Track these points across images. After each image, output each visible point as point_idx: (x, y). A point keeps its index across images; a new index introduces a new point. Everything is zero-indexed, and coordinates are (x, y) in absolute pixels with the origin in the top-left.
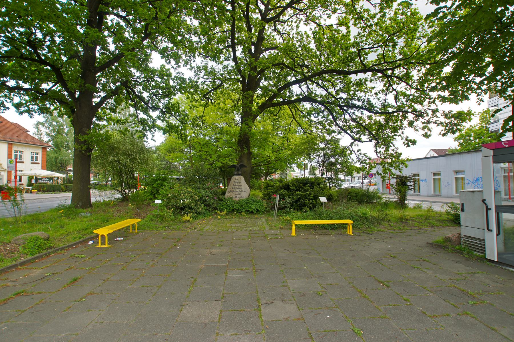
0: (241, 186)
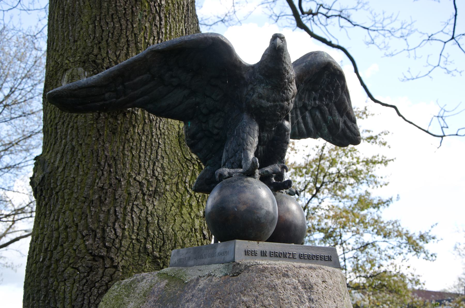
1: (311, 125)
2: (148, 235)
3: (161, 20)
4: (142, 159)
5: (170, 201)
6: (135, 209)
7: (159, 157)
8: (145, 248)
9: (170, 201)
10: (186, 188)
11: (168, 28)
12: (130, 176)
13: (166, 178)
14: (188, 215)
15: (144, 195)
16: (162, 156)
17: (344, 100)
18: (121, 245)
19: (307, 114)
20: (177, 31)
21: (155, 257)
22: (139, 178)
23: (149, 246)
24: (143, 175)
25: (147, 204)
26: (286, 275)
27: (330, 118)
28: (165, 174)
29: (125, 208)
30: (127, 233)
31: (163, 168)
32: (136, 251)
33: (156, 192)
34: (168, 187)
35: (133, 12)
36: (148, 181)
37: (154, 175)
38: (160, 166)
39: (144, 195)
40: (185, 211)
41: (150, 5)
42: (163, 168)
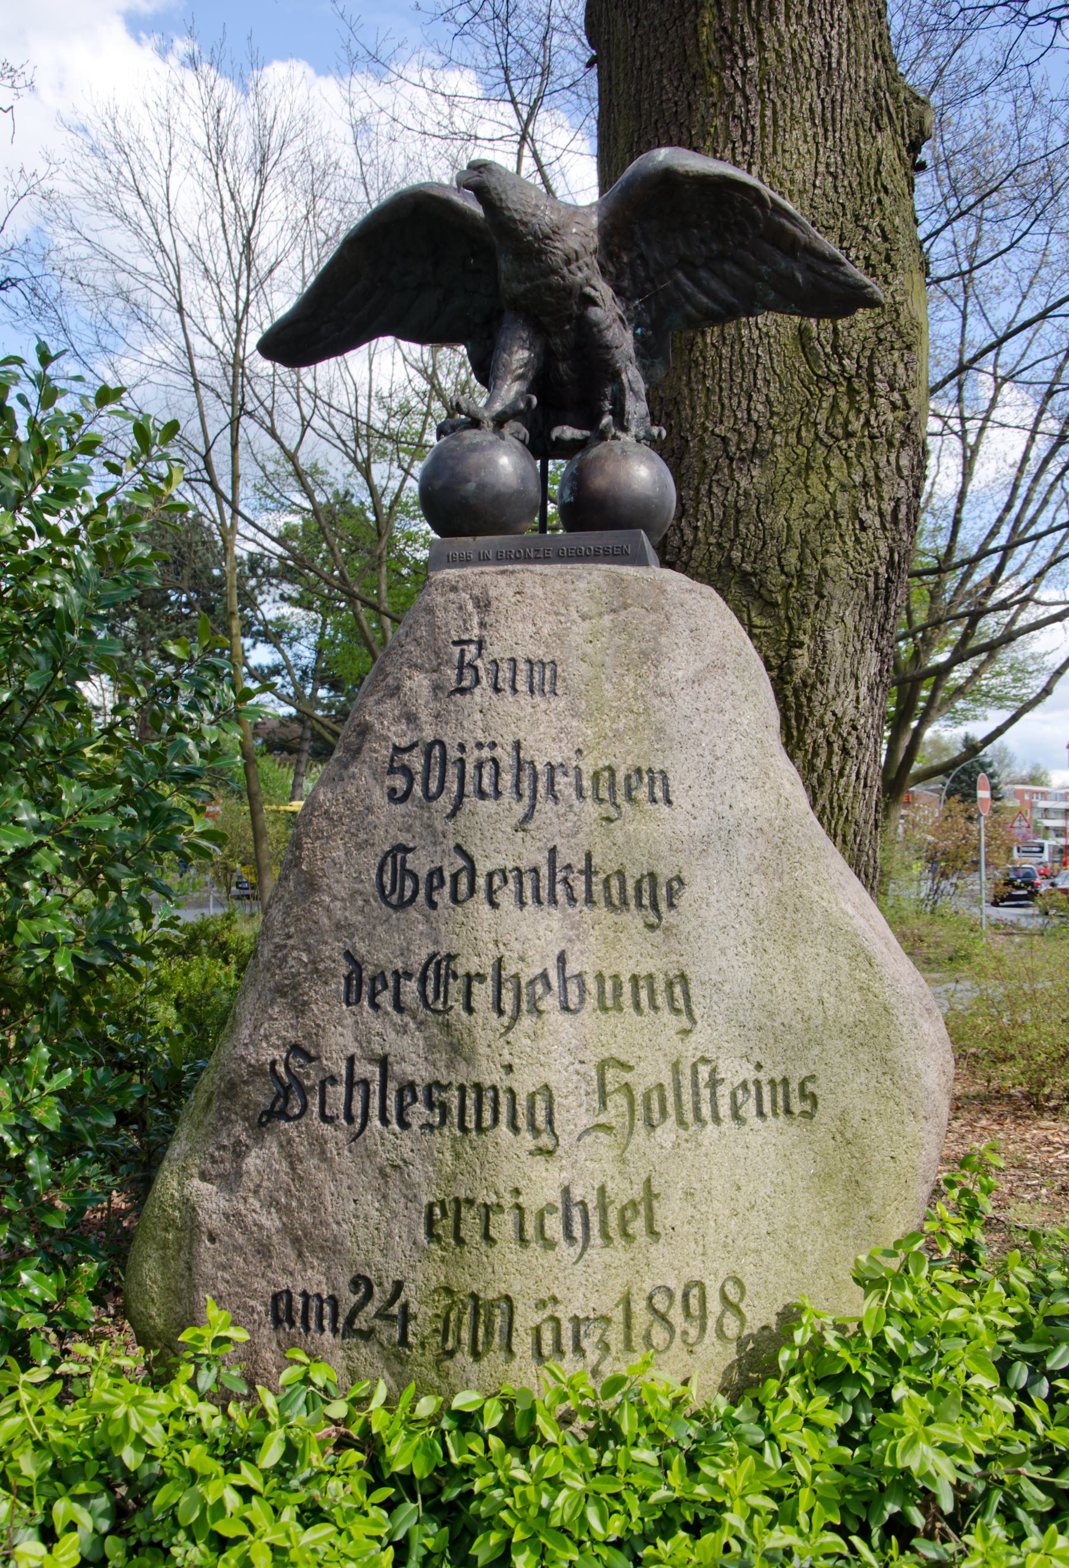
0: (654, 895)
1: (725, 294)
2: (737, 534)
3: (747, 100)
4: (725, 393)
5: (783, 464)
6: (715, 490)
7: (760, 383)
8: (729, 559)
9: (783, 464)
10: (817, 437)
11: (769, 113)
12: (705, 430)
13: (775, 421)
14: (821, 487)
15: (731, 460)
16: (765, 379)
17: (782, 226)
18: (691, 558)
19: (703, 274)
20: (796, 112)
21: (745, 574)
22: (720, 430)
23: (736, 555)
24: (729, 423)
25: (737, 475)
26: (454, 589)
27: (764, 268)
28: (772, 414)
29: (697, 490)
30: (700, 534)
31: (768, 402)
32: (715, 565)
33: (754, 452)
34: (778, 439)
35: (690, 105)
36: (740, 433)
37: (750, 419)
38: (763, 399)
39: (731, 460)
40: (813, 479)
41: (720, 79)
42: (768, 402)
